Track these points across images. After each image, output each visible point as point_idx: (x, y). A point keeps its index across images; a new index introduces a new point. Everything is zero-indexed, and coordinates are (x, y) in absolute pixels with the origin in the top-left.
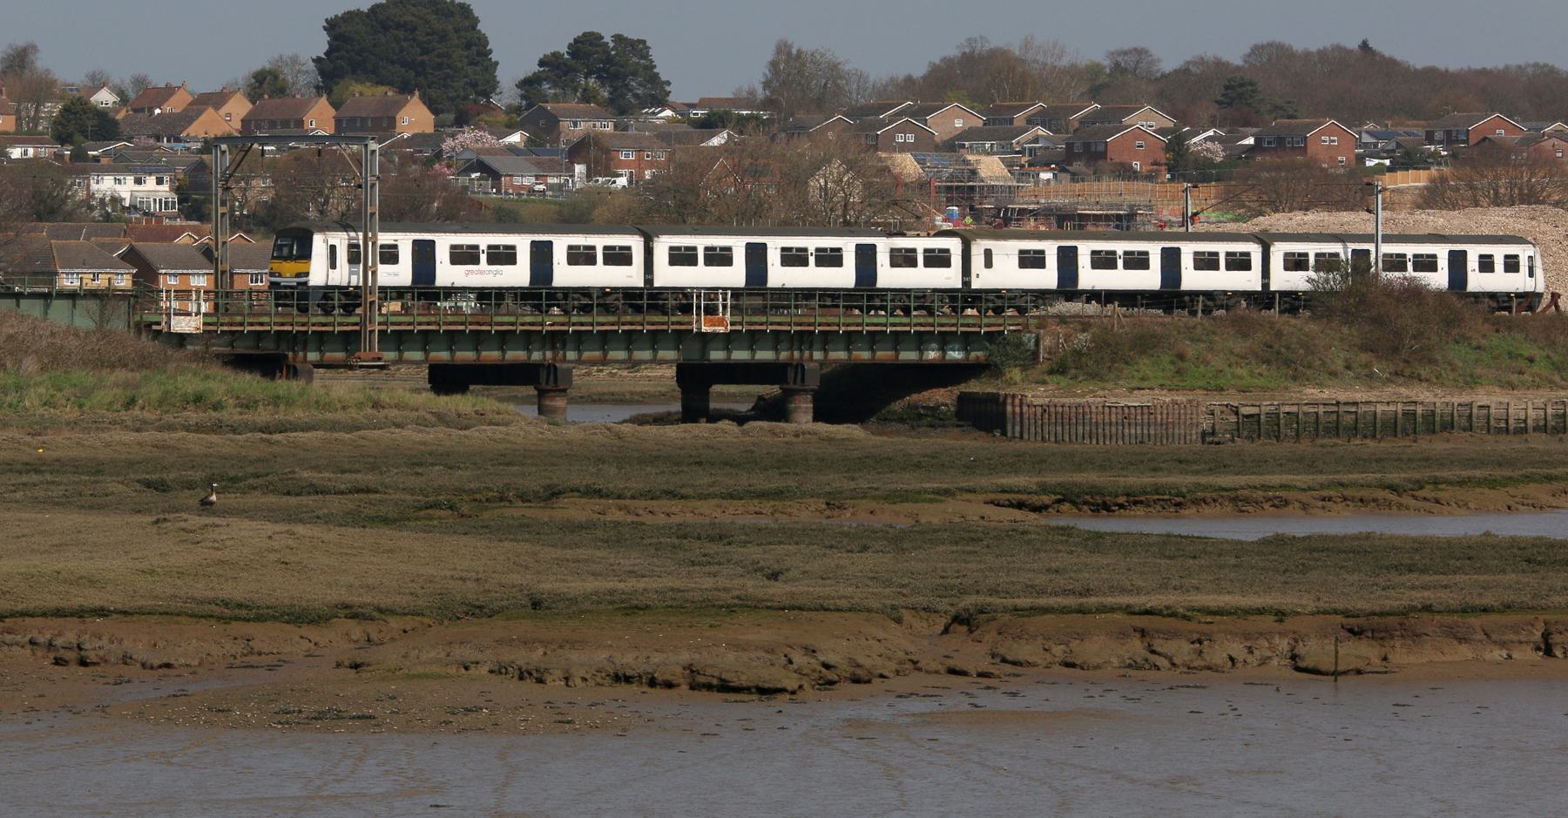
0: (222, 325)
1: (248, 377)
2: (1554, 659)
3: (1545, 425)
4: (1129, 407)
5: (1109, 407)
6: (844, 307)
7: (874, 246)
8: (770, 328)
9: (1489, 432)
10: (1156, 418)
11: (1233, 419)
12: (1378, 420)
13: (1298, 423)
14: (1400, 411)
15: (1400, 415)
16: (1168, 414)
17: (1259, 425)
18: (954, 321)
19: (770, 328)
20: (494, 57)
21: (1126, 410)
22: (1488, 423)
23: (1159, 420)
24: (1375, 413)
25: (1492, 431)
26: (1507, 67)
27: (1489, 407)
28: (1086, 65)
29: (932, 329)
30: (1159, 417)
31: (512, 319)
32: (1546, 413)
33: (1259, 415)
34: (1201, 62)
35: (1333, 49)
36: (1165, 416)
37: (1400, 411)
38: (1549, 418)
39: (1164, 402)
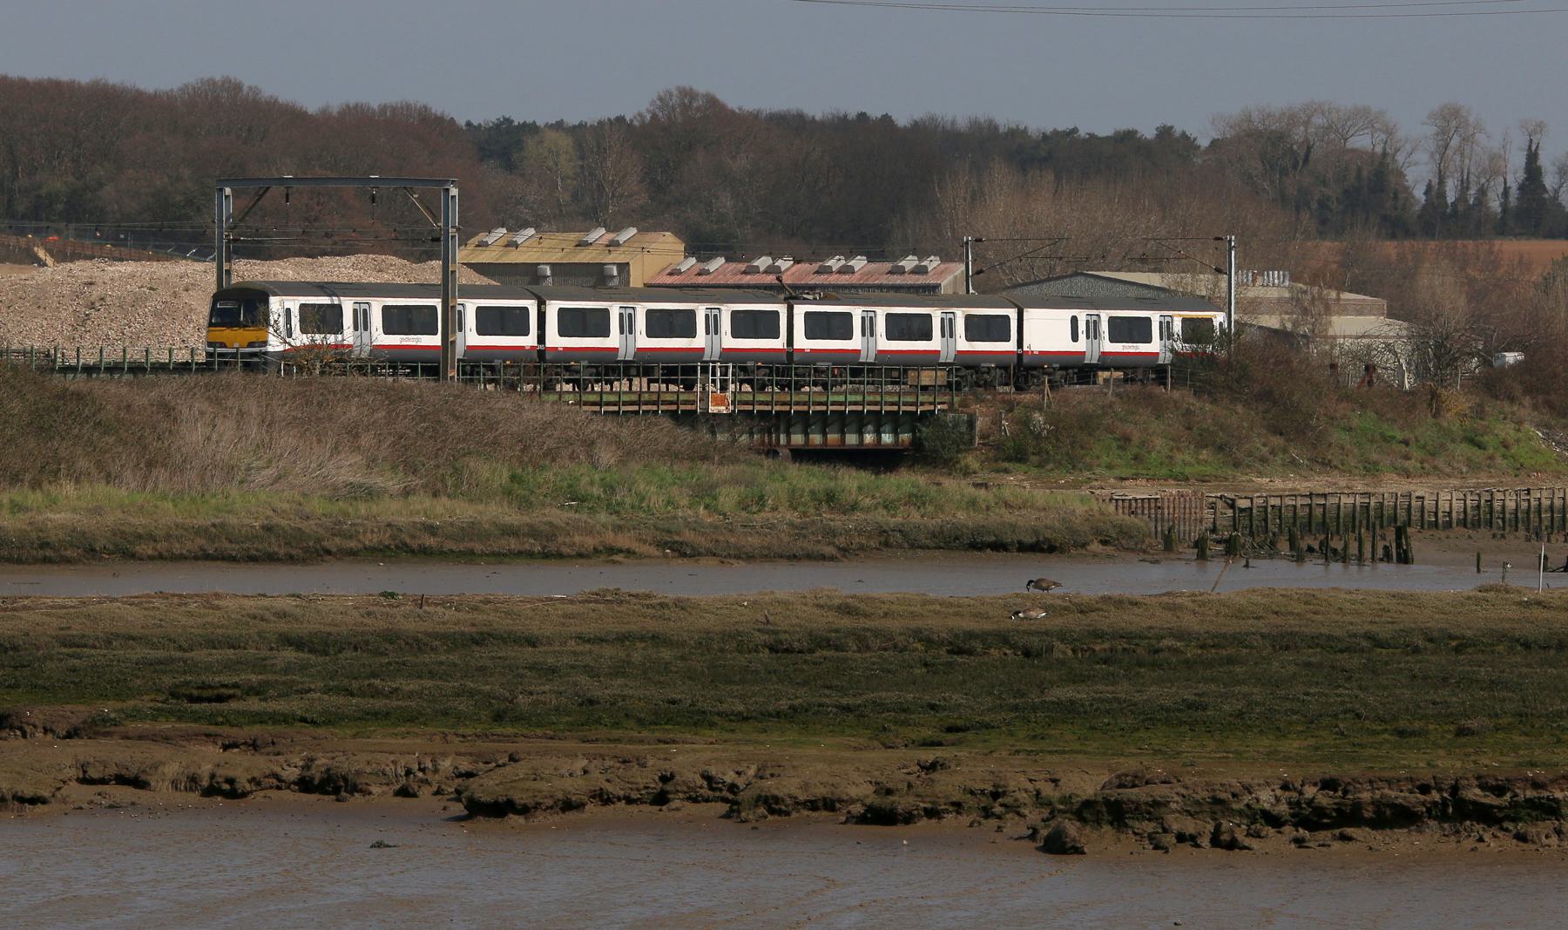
0: (922, 404)
1: (863, 474)
2: (1081, 856)
3: (1465, 519)
4: (1136, 500)
5: (1117, 500)
6: (484, 366)
7: (929, 316)
8: (794, 408)
9: (1422, 527)
10: (1163, 514)
11: (1230, 512)
12: (1342, 514)
13: (1280, 518)
14: (1358, 503)
15: (1358, 508)
16: (1174, 508)
17: (1251, 520)
18: (824, 399)
19: (794, 408)
20: (852, 113)
21: (1134, 504)
22: (1422, 516)
23: (1166, 515)
24: (1339, 507)
25: (1426, 526)
26: (324, 111)
27: (1423, 498)
28: (114, 85)
29: (824, 408)
30: (1166, 511)
31: (859, 398)
32: (1465, 504)
33: (1251, 509)
34: (73, 82)
35: (223, 82)
36: (1171, 510)
37: (1358, 503)
38: (1469, 510)
39: (1171, 495)
